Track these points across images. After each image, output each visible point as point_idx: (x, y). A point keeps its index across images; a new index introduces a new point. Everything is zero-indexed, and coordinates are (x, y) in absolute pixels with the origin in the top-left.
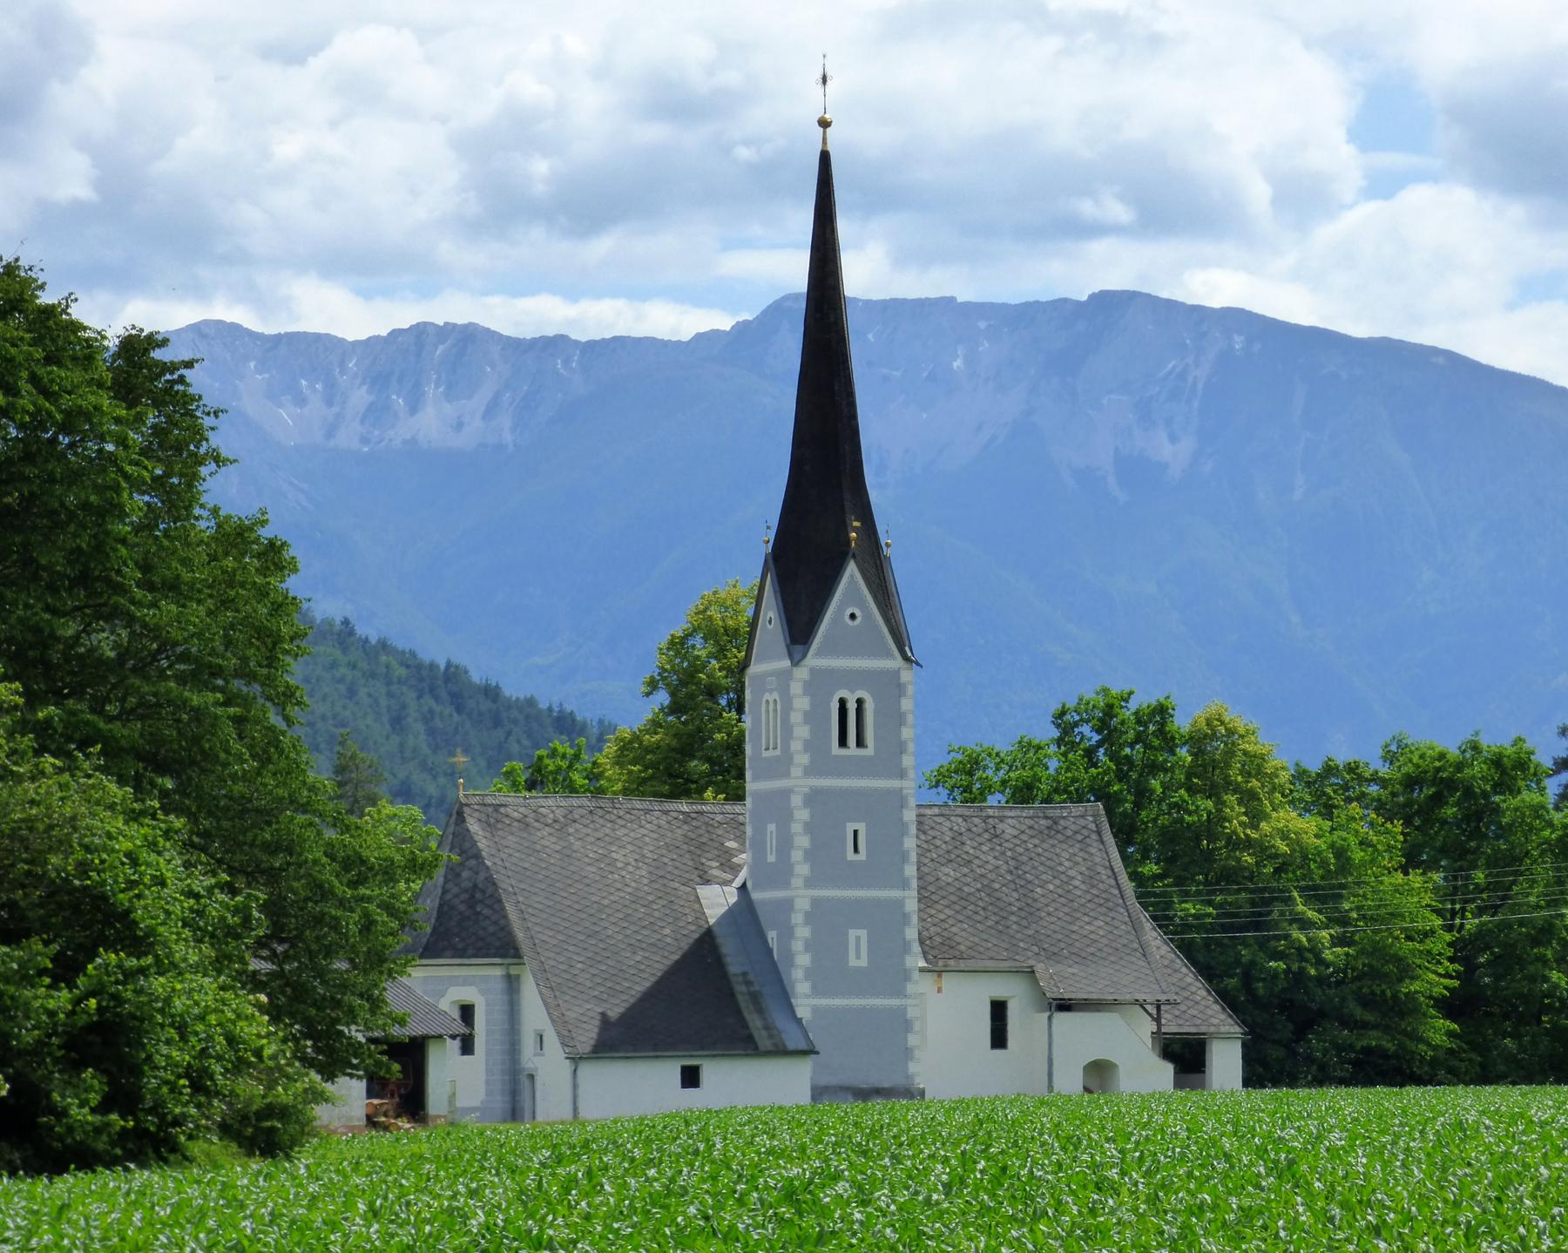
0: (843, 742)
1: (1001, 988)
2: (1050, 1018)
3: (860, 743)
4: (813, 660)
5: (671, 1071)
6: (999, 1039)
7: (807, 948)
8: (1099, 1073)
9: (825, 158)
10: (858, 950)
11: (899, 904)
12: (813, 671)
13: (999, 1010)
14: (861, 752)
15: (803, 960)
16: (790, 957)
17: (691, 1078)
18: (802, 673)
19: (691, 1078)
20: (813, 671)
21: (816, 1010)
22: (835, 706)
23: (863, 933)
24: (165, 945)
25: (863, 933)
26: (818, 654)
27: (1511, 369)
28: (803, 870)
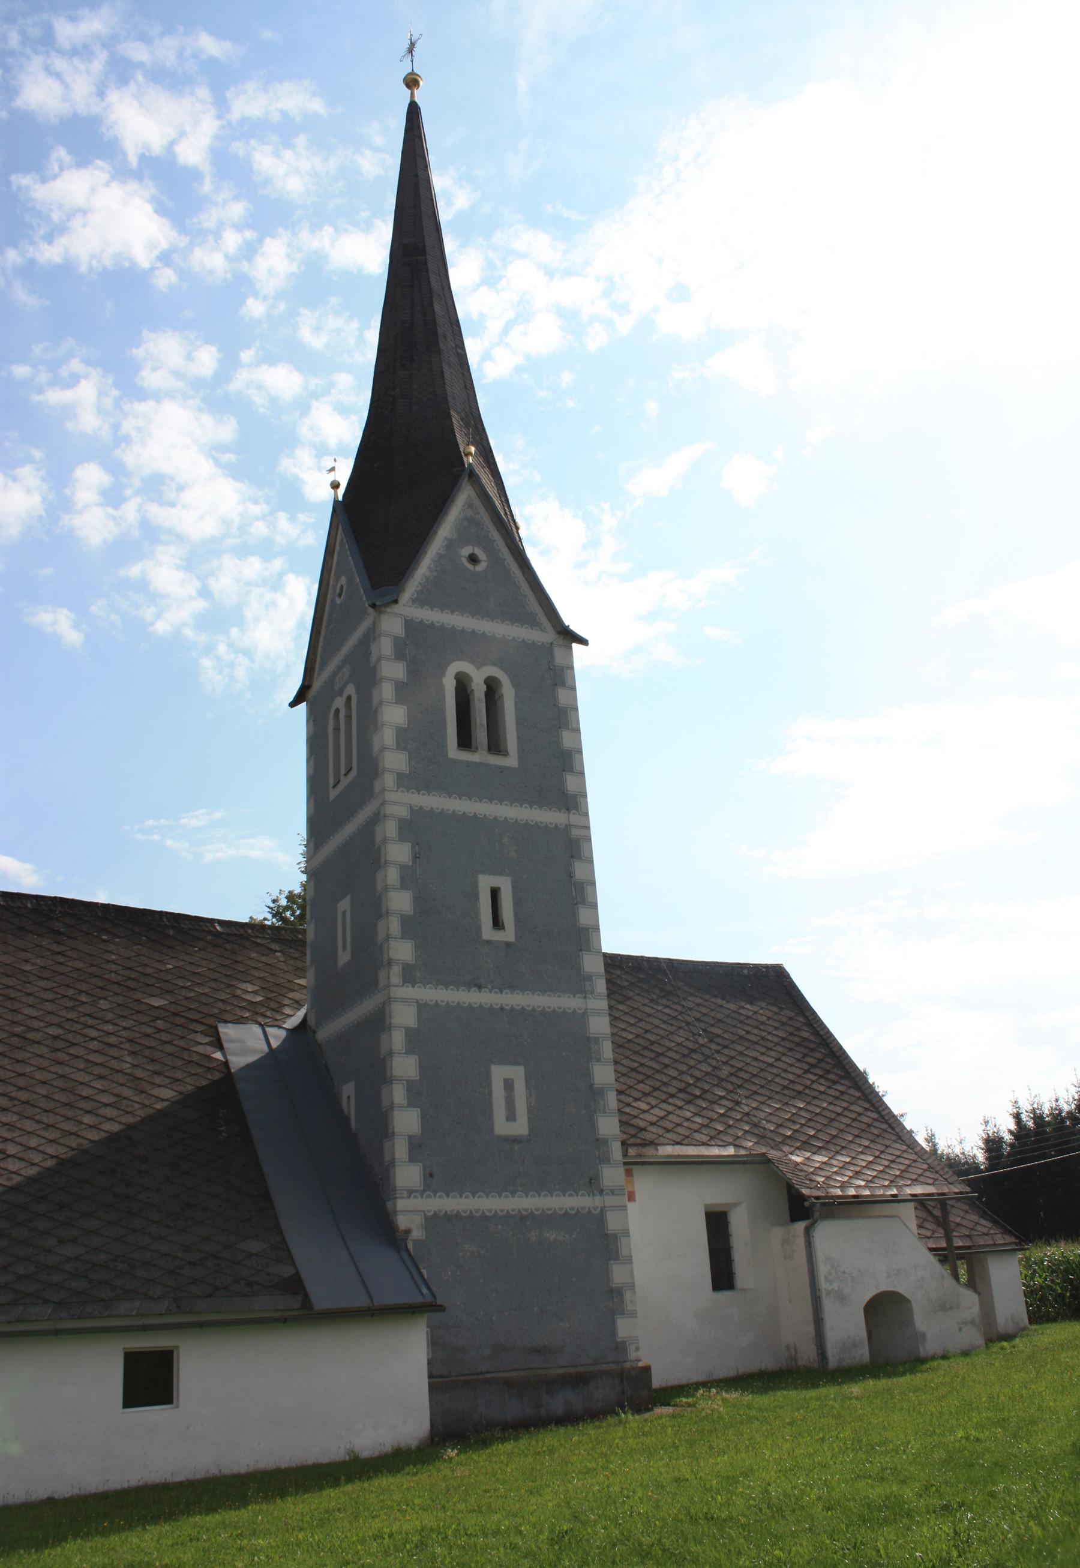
0: (465, 741)
1: (716, 1191)
2: (808, 1231)
3: (496, 746)
4: (408, 608)
5: (94, 1373)
6: (723, 1276)
7: (402, 743)
8: (185, 1553)
9: (414, 113)
10: (510, 1098)
11: (579, 1019)
12: (409, 624)
13: (717, 1223)
14: (495, 760)
15: (407, 1121)
16: (380, 1124)
17: (149, 1381)
18: (391, 624)
19: (149, 1381)
20: (409, 624)
21: (433, 1221)
22: (449, 684)
23: (502, 1127)
24: (415, 1474)
25: (502, 1127)
26: (422, 600)
27: (793, 976)
28: (402, 951)
